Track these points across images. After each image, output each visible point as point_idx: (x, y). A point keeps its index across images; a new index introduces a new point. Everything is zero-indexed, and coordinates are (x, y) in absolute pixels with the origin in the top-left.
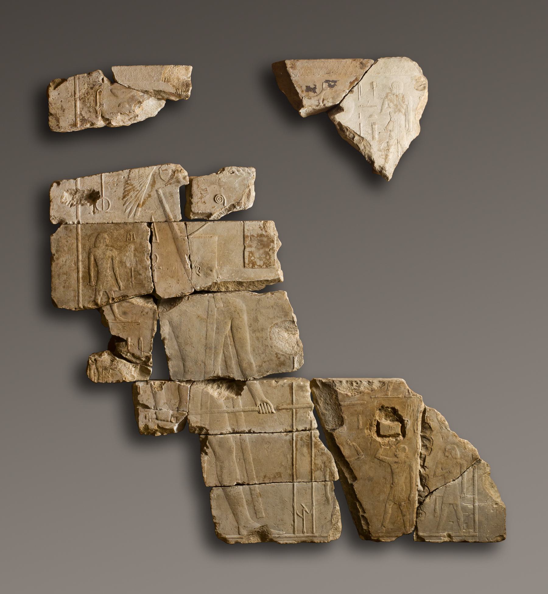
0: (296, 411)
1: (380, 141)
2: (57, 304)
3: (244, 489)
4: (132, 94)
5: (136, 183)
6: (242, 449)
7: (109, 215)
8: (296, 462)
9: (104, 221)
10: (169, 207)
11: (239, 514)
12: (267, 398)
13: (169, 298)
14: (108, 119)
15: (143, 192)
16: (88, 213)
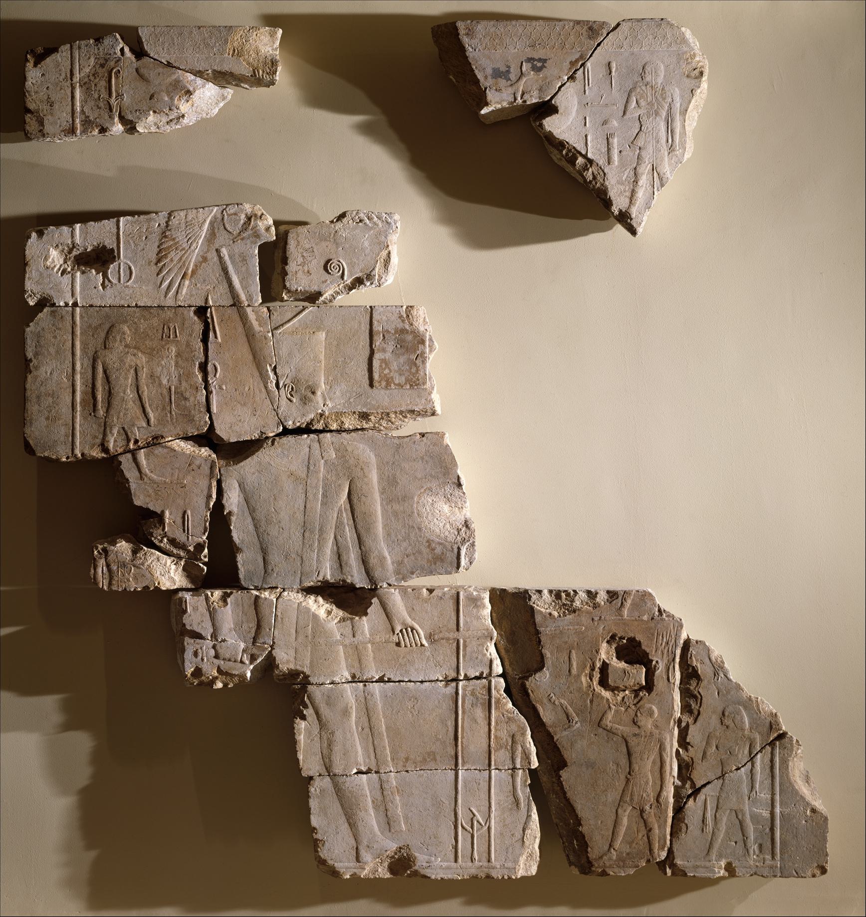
0: (465, 642)
1: (623, 165)
2: (35, 449)
3: (369, 780)
4: (174, 77)
5: (180, 236)
6: (367, 710)
7: (131, 291)
8: (462, 734)
9: (122, 302)
10: (240, 281)
11: (360, 824)
12: (414, 619)
13: (238, 442)
14: (131, 122)
15: (194, 251)
16: (93, 287)
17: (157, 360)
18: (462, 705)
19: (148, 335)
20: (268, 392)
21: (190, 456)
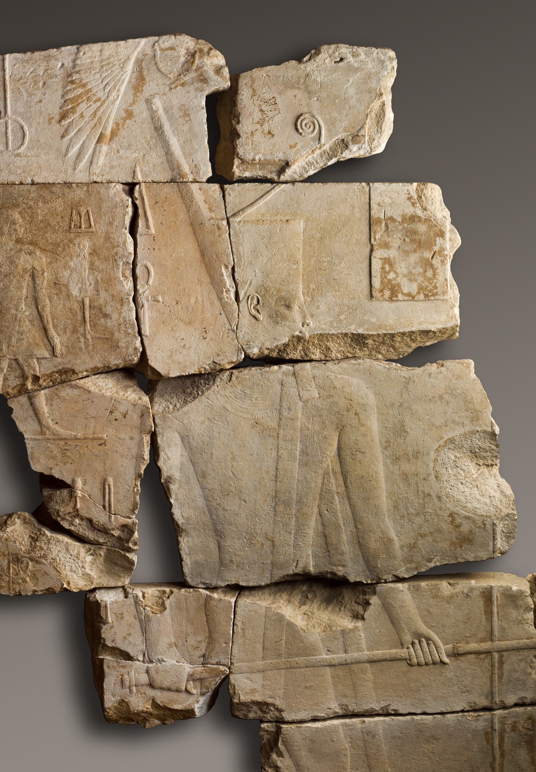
7: (24, 162)
12: (431, 627)
17: (63, 261)
18: (500, 745)
19: (49, 224)
20: (224, 305)
21: (112, 399)
